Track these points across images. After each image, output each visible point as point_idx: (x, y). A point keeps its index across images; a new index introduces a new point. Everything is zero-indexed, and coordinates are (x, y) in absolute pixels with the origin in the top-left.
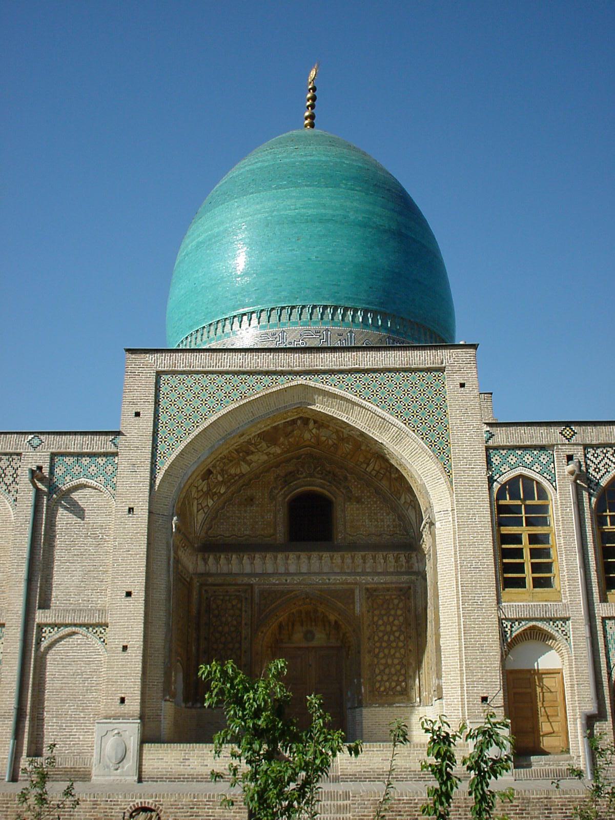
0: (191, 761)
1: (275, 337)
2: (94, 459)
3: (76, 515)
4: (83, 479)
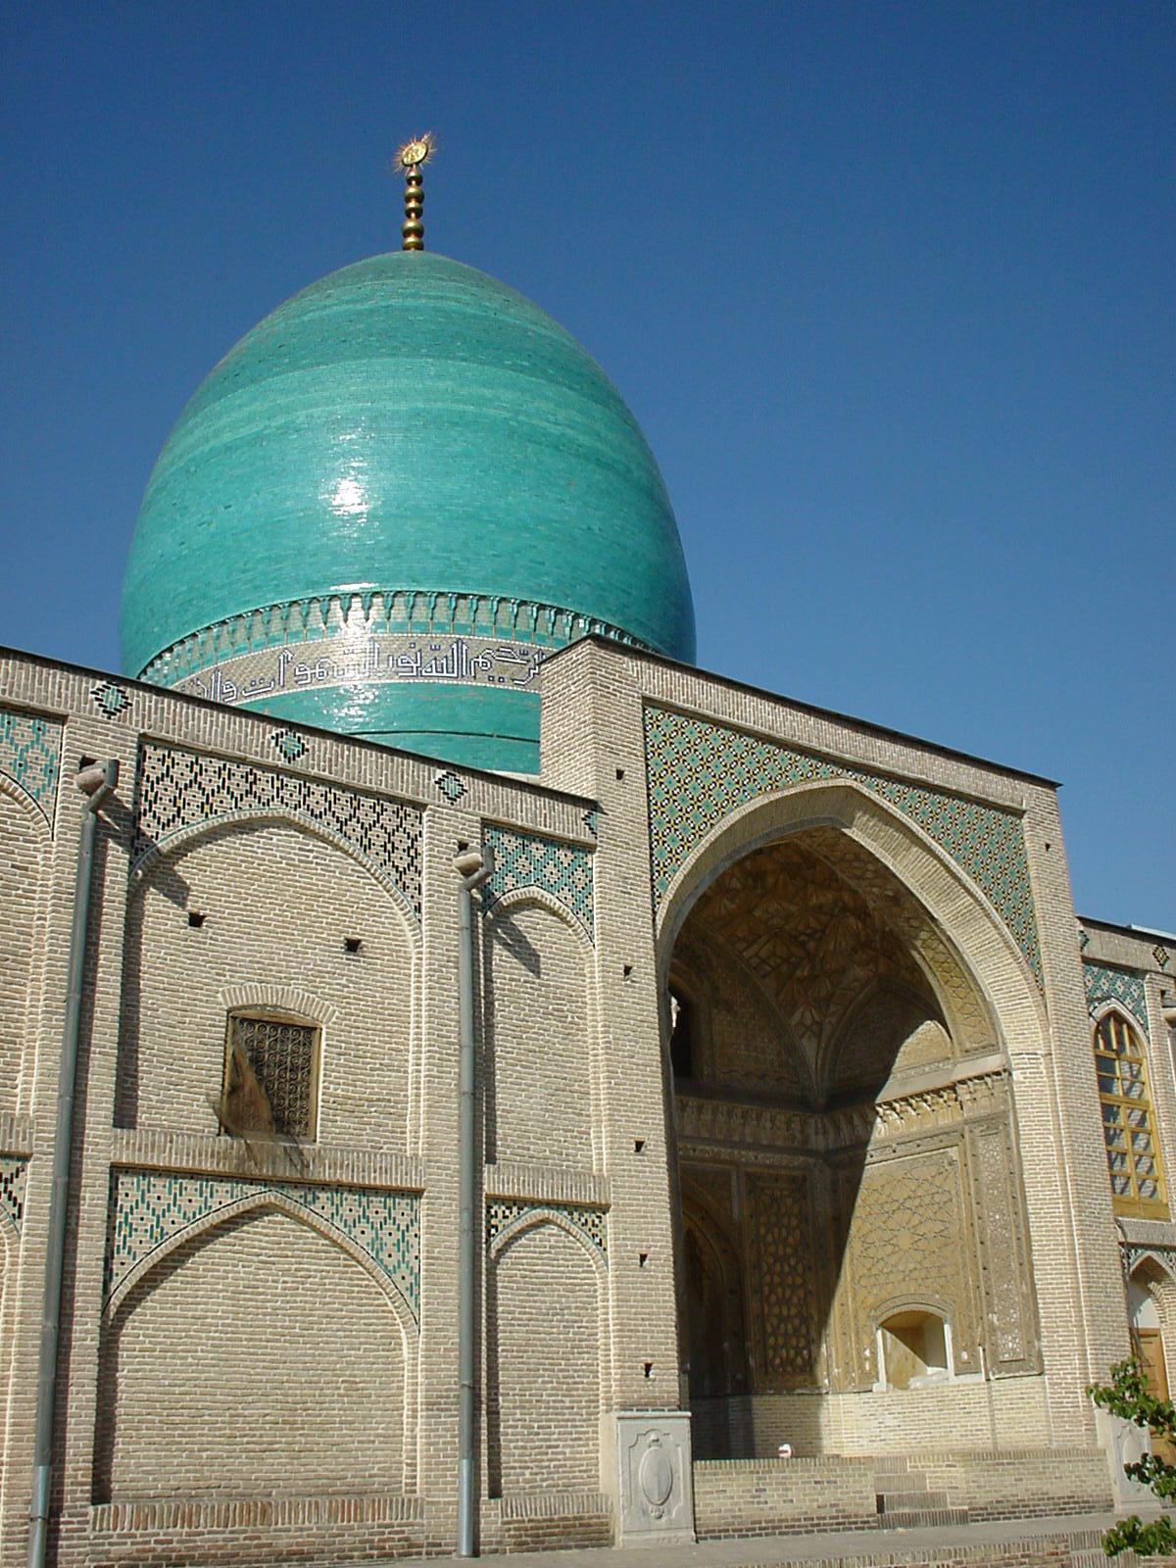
0: (768, 1492)
1: (526, 658)
2: (552, 849)
3: (525, 964)
4: (534, 888)
